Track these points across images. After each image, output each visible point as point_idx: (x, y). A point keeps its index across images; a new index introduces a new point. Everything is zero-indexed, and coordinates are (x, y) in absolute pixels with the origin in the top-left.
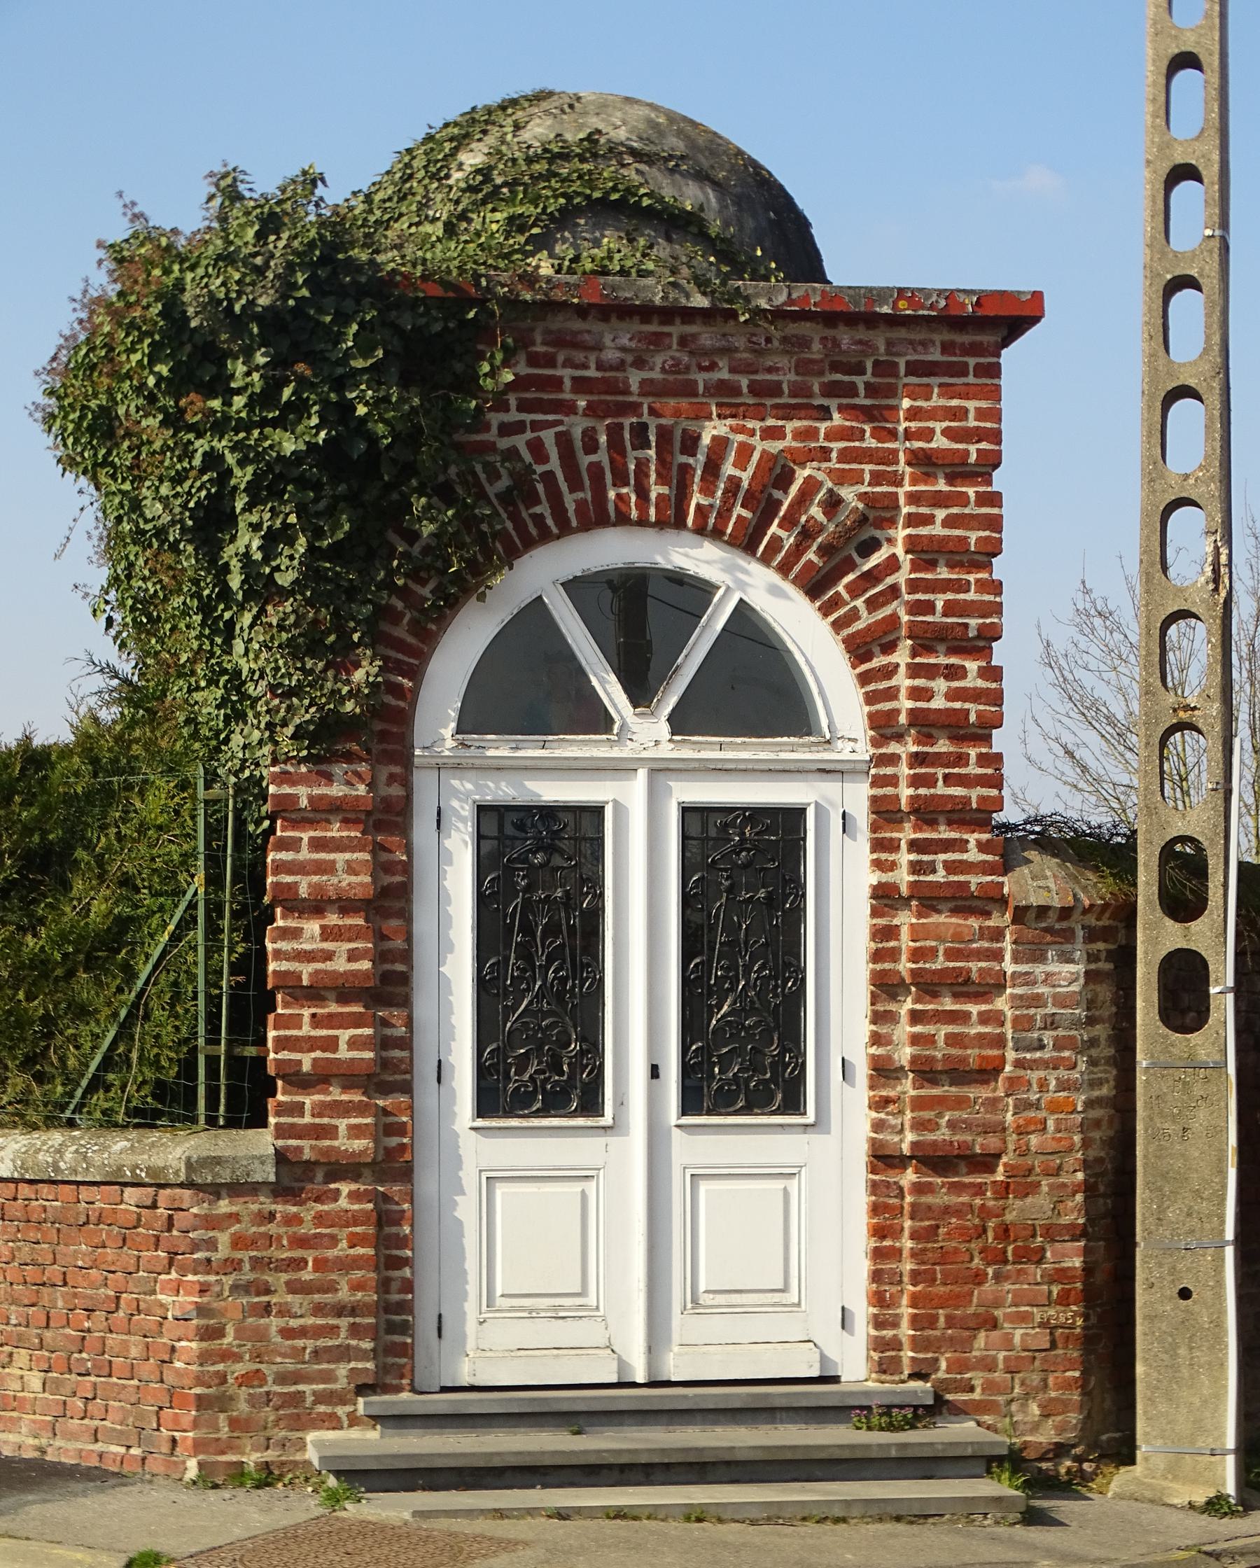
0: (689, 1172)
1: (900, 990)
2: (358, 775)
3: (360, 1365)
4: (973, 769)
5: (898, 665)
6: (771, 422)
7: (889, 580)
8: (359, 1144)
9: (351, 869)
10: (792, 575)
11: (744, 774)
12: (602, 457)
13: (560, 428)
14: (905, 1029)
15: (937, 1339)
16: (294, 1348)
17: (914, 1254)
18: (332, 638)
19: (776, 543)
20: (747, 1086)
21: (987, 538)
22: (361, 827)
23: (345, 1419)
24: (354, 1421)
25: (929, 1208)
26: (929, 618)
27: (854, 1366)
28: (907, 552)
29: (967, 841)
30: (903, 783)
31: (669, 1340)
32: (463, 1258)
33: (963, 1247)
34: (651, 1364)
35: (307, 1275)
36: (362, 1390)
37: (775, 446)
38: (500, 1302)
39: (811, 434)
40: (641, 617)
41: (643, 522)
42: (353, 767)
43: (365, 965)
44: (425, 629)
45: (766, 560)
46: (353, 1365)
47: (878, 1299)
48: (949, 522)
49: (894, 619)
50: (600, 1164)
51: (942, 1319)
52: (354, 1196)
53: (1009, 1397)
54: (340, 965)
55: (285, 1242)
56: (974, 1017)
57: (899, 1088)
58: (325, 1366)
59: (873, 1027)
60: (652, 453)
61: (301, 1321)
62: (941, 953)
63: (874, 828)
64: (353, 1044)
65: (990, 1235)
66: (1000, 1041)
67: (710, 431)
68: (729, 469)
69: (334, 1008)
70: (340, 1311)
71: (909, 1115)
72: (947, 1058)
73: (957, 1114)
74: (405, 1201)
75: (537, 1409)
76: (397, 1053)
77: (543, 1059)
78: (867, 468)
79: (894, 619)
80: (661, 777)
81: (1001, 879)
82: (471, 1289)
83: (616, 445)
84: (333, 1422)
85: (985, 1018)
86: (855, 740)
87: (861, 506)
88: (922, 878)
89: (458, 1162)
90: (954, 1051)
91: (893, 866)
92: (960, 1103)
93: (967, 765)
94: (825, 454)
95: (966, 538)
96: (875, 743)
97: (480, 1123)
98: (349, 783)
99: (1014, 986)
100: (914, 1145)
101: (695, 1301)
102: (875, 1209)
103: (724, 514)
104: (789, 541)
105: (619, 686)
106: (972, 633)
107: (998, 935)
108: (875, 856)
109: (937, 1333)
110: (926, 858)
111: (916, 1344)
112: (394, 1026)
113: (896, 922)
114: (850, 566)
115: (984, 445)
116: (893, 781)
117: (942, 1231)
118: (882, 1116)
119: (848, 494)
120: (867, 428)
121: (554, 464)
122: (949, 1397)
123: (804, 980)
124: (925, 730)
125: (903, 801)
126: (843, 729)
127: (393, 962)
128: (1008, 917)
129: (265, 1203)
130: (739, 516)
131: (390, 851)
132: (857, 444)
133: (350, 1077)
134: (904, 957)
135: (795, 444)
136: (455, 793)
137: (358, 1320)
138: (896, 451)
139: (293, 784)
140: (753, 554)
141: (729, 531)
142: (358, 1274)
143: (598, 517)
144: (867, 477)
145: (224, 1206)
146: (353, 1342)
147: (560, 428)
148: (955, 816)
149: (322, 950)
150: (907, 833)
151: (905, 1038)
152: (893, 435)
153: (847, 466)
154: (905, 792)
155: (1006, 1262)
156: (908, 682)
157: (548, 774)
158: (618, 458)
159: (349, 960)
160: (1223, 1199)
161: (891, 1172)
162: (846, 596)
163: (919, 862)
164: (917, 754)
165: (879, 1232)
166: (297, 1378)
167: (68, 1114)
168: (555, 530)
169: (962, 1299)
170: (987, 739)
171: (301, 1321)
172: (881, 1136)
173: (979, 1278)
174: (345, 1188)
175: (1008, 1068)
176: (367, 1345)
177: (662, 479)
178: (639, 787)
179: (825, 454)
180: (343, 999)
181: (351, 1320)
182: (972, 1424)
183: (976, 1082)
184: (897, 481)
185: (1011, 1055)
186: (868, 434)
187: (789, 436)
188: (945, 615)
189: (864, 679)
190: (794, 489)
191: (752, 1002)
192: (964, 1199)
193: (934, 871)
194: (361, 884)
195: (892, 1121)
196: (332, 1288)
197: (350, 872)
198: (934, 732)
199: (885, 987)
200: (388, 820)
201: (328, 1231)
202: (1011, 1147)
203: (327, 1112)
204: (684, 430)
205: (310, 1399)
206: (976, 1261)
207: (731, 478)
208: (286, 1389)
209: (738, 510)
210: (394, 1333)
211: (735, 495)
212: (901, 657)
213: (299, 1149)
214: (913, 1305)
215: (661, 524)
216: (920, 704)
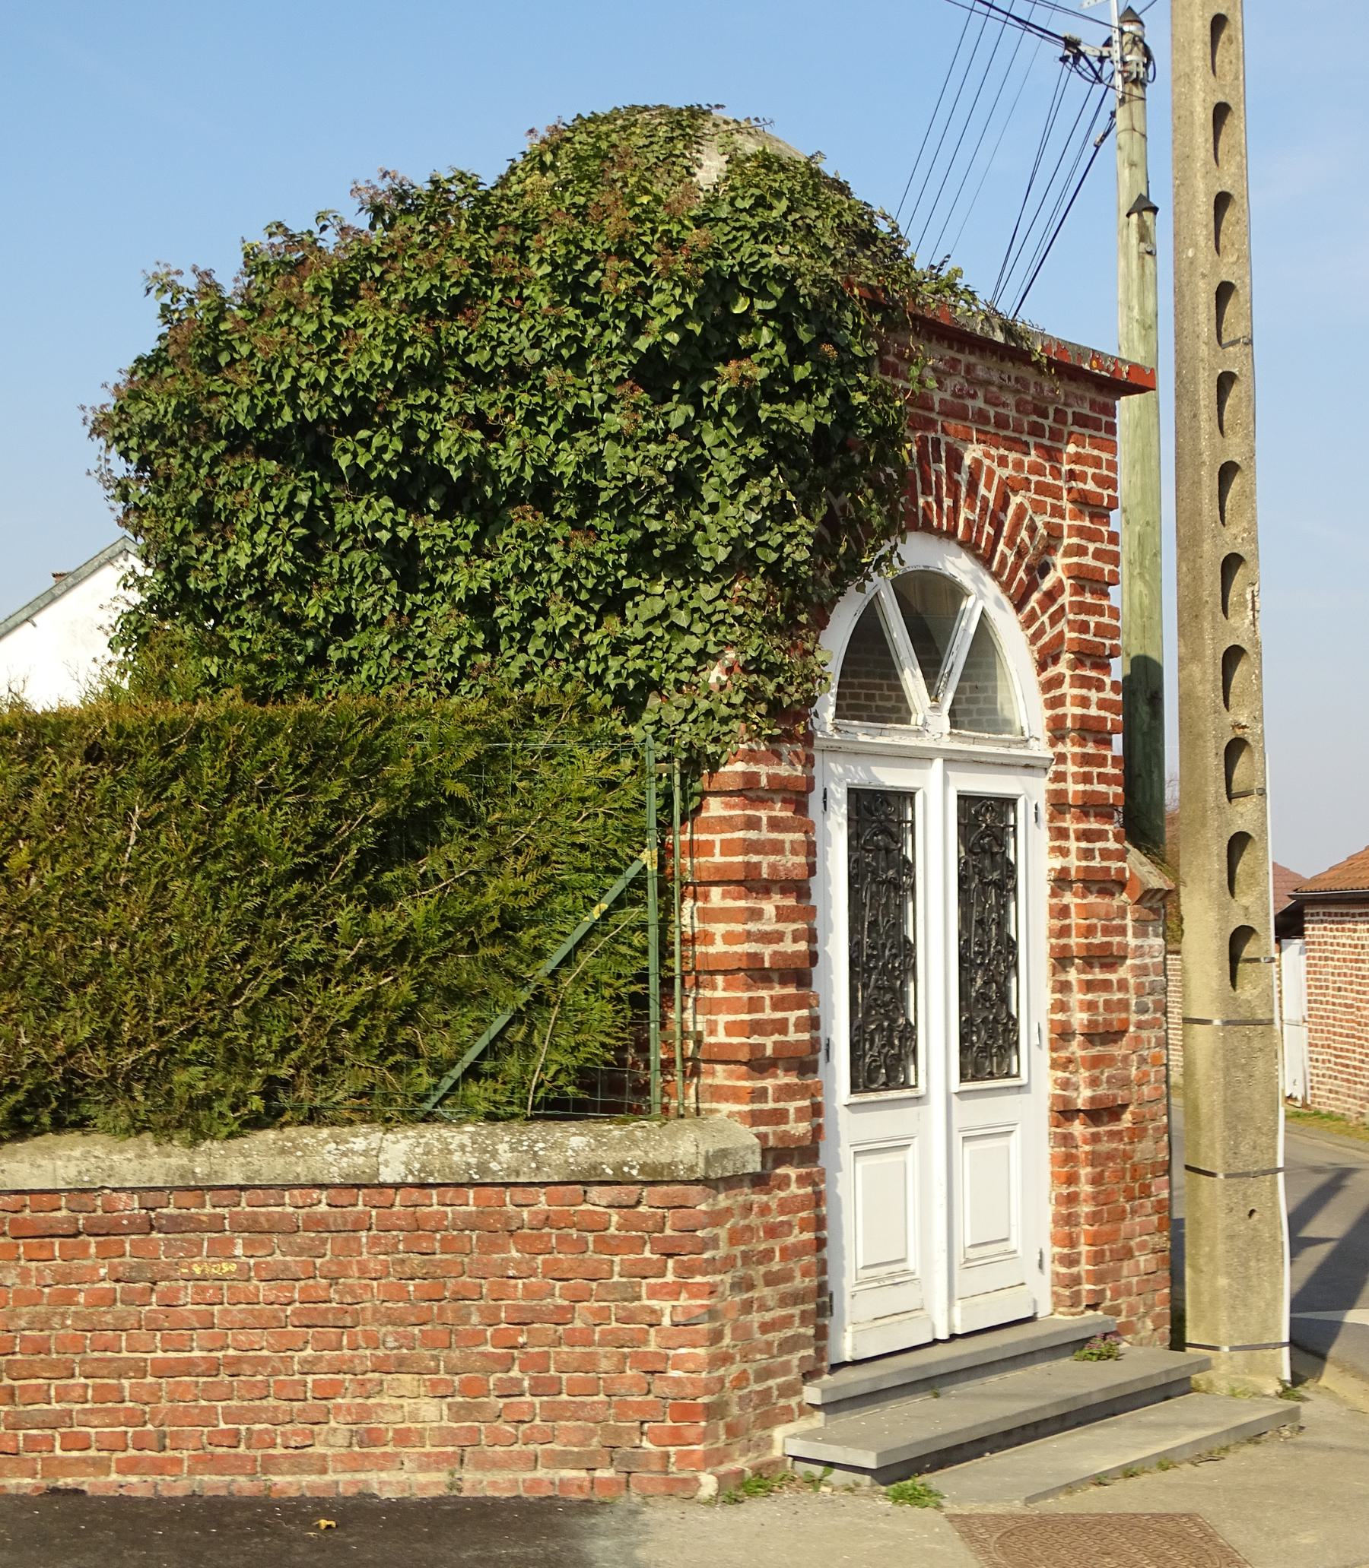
14: (1077, 997)
60: (943, 466)
63: (1052, 819)
129: (747, 1195)
139: (757, 762)
145: (723, 1201)
160: (1276, 1132)
167: (428, 1106)
175: (1132, 1029)
199: (1061, 959)
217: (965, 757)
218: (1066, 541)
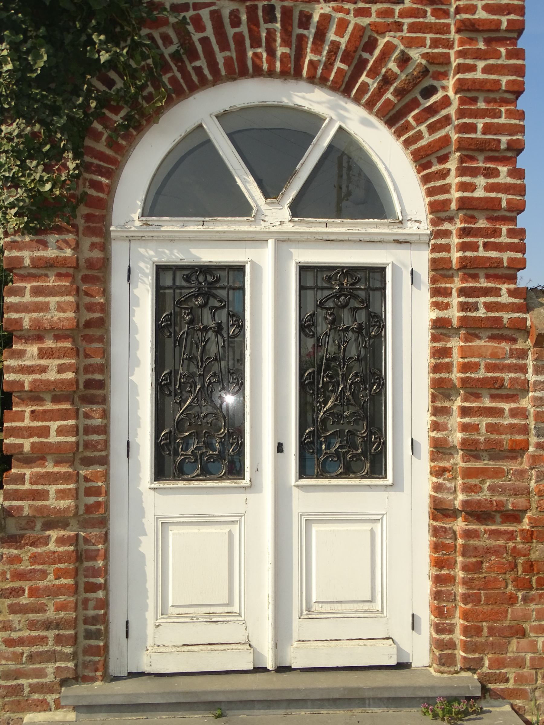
0: (304, 518)
1: (452, 392)
2: (66, 242)
3: (63, 665)
4: (504, 239)
5: (449, 170)
6: (361, 5)
7: (444, 113)
8: (64, 504)
9: (60, 308)
10: (376, 109)
11: (342, 244)
12: (244, 28)
13: (213, 8)
15: (482, 644)
16: (14, 653)
17: (465, 582)
18: (48, 147)
19: (364, 87)
20: (345, 458)
21: (514, 81)
22: (70, 279)
23: (52, 704)
24: (58, 706)
25: (476, 548)
26: (473, 136)
27: (420, 651)
28: (456, 93)
29: (500, 289)
30: (454, 249)
31: (291, 638)
32: (145, 581)
33: (500, 577)
34: (276, 656)
35: (24, 600)
36: (64, 682)
37: (364, 21)
38: (172, 611)
39: (389, 13)
40: (273, 144)
41: (271, 74)
42: (63, 237)
43: (70, 375)
44: (117, 143)
45: (357, 100)
46: (58, 664)
47: (439, 612)
48: (486, 70)
49: (446, 139)
50: (242, 512)
51: (485, 630)
52: (61, 541)
53: (534, 686)
54: (52, 375)
55: (8, 576)
56: (507, 412)
57: (452, 461)
58: (37, 666)
59: (434, 418)
60: (278, 25)
61: (20, 634)
62: (482, 366)
63: (433, 280)
64: (60, 431)
65: (520, 569)
66: (525, 430)
67: (319, 10)
68: (331, 36)
69: (49, 406)
70: (48, 625)
71: (460, 481)
72: (488, 441)
73: (495, 481)
74: (99, 543)
75: (189, 700)
76: (95, 437)
77: (200, 445)
78: (429, 36)
79: (446, 139)
80: (284, 246)
81: (525, 316)
82: (151, 602)
83: (253, 21)
84: (43, 706)
85: (514, 413)
86: (420, 222)
87: (424, 62)
88: (468, 314)
89: (142, 513)
90: (493, 436)
91: (447, 306)
92: (498, 473)
93: (500, 236)
94: (399, 27)
95: (499, 81)
96: (434, 223)
97: (157, 485)
98: (59, 248)
99: (535, 391)
100: (465, 503)
101: (309, 611)
102: (436, 547)
103: (328, 66)
104: (373, 85)
105: (255, 184)
106: (503, 146)
107: (523, 354)
108: (434, 299)
109: (482, 640)
110: (471, 300)
111: (467, 648)
112: (93, 418)
113: (449, 345)
114: (415, 103)
115: (512, 17)
116: (447, 248)
117: (485, 565)
118: (441, 481)
119: (415, 54)
120: (429, 9)
121: (209, 32)
122: (491, 686)
123: (384, 385)
124: (470, 213)
125: (454, 262)
126: (411, 214)
127: (93, 373)
128: (529, 343)
130: (339, 68)
131: (92, 296)
132: (421, 20)
133: (61, 454)
134: (455, 370)
135: (378, 20)
136: (142, 257)
137: (61, 632)
138: (448, 25)
139: (20, 249)
140: (349, 96)
141: (331, 78)
142: (61, 599)
143: (240, 71)
144: (428, 42)
146: (58, 648)
147: (213, 8)
148: (491, 272)
149: (39, 366)
150: (456, 284)
151: (456, 426)
152: (446, 14)
153: (414, 35)
154: (455, 255)
155: (531, 588)
156: (459, 179)
157: (205, 243)
158: (255, 28)
159: (58, 372)
161: (446, 520)
162: (413, 123)
163: (467, 303)
164: (464, 228)
165: (438, 564)
166: (18, 675)
168: (210, 77)
169: (501, 615)
170: (513, 220)
171: (20, 634)
172: (439, 495)
173: (512, 600)
174: (54, 534)
175: (531, 449)
176: (68, 650)
177: (286, 42)
178: (269, 252)
179: (399, 27)
180: (56, 399)
181: (57, 632)
182: (508, 708)
183: (507, 457)
184: (449, 45)
185: (533, 440)
186: (429, 14)
187: (374, 14)
188: (484, 133)
189: (426, 179)
190: (377, 52)
191: (348, 400)
192: (501, 542)
193: (477, 309)
194: (68, 319)
195: (448, 484)
196: (42, 609)
197: (59, 309)
198: (475, 213)
199: (441, 389)
200: (92, 276)
201: (40, 567)
202: (534, 505)
203: (42, 481)
204: (301, 12)
205: (27, 690)
206: (510, 587)
207: (333, 42)
208: (9, 683)
209: (338, 64)
210: (89, 639)
211: (336, 54)
212: (452, 164)
213: (21, 508)
214: (465, 618)
215: (284, 74)
216: (466, 194)
217: (309, 236)
218: (454, 64)
